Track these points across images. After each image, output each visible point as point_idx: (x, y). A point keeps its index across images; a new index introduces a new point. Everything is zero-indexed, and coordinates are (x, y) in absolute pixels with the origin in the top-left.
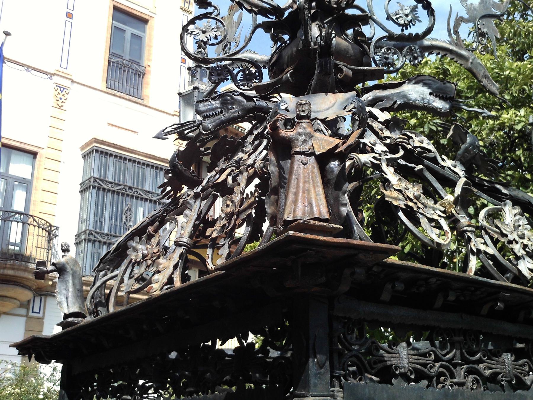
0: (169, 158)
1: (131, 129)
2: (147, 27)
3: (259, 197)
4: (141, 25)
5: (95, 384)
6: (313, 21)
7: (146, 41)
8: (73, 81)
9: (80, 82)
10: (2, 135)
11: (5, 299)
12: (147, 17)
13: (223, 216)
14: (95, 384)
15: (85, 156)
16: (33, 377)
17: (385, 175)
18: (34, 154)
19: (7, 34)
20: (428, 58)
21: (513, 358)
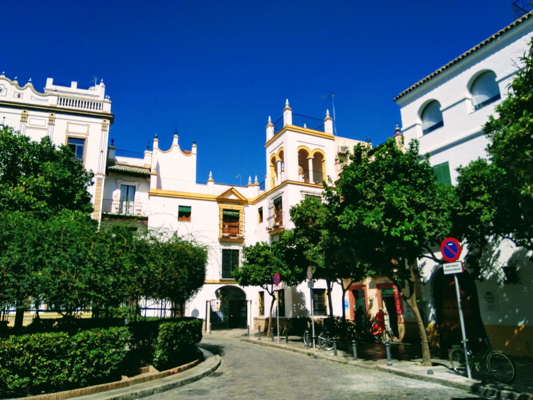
0: (444, 114)
1: (507, 75)
2: (85, 142)
3: (133, 281)
4: (82, 141)
5: (395, 271)
6: (472, 191)
7: (85, 148)
9: (409, 126)
10: (110, 105)
11: (212, 282)
13: (281, 227)
14: (395, 271)
15: (269, 209)
16: (505, 175)
17: (493, 385)
19: (4, 118)
20: (490, 389)
21: (145, 297)
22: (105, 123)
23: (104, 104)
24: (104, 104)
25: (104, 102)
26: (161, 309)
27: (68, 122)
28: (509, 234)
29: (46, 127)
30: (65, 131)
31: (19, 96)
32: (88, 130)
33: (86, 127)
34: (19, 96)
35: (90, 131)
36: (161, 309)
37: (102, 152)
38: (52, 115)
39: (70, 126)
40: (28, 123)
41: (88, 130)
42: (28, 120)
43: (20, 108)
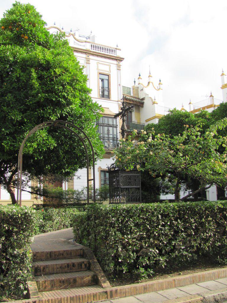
39: (99, 65)
43: (116, 60)
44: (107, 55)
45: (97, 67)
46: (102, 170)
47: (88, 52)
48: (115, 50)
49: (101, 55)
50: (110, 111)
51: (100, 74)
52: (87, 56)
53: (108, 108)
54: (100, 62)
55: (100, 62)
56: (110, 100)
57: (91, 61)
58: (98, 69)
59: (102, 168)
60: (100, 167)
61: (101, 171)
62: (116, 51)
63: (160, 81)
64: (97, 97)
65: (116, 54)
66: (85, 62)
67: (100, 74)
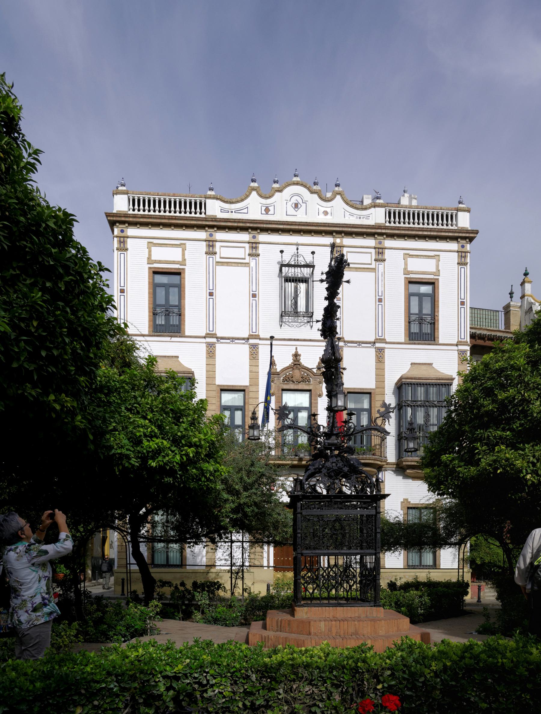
8: (217, 338)
12: (178, 271)
18: (244, 391)
22: (463, 250)
23: (207, 201)
24: (207, 201)
25: (458, 210)
26: (130, 564)
27: (149, 242)
28: (181, 442)
29: (373, 266)
30: (146, 261)
31: (267, 210)
32: (438, 266)
33: (433, 261)
34: (267, 210)
35: (186, 257)
36: (130, 564)
37: (463, 303)
38: (254, 237)
39: (410, 260)
40: (218, 256)
41: (438, 266)
42: (217, 249)
43: (454, 239)
44: (431, 230)
45: (147, 256)
46: (411, 506)
47: (379, 231)
48: (203, 200)
49: (414, 233)
50: (184, 367)
51: (410, 282)
52: (251, 235)
53: (431, 364)
54: (411, 252)
55: (411, 252)
56: (436, 345)
57: (130, 243)
58: (150, 261)
59: (412, 502)
60: (407, 500)
61: (408, 508)
62: (456, 215)
63: (526, 274)
64: (403, 341)
65: (205, 214)
66: (374, 258)
67: (410, 282)
